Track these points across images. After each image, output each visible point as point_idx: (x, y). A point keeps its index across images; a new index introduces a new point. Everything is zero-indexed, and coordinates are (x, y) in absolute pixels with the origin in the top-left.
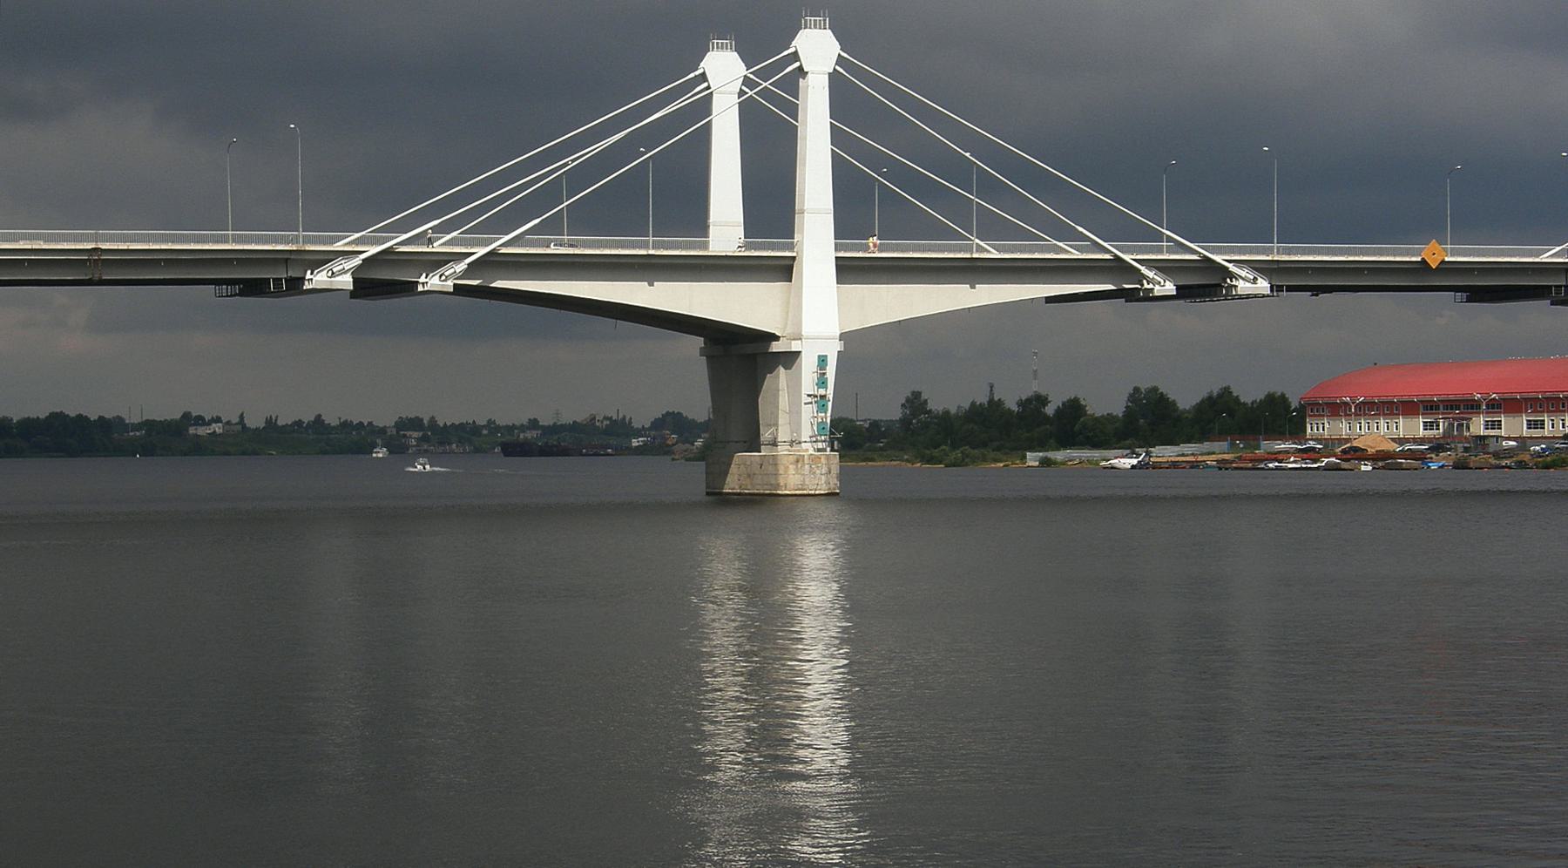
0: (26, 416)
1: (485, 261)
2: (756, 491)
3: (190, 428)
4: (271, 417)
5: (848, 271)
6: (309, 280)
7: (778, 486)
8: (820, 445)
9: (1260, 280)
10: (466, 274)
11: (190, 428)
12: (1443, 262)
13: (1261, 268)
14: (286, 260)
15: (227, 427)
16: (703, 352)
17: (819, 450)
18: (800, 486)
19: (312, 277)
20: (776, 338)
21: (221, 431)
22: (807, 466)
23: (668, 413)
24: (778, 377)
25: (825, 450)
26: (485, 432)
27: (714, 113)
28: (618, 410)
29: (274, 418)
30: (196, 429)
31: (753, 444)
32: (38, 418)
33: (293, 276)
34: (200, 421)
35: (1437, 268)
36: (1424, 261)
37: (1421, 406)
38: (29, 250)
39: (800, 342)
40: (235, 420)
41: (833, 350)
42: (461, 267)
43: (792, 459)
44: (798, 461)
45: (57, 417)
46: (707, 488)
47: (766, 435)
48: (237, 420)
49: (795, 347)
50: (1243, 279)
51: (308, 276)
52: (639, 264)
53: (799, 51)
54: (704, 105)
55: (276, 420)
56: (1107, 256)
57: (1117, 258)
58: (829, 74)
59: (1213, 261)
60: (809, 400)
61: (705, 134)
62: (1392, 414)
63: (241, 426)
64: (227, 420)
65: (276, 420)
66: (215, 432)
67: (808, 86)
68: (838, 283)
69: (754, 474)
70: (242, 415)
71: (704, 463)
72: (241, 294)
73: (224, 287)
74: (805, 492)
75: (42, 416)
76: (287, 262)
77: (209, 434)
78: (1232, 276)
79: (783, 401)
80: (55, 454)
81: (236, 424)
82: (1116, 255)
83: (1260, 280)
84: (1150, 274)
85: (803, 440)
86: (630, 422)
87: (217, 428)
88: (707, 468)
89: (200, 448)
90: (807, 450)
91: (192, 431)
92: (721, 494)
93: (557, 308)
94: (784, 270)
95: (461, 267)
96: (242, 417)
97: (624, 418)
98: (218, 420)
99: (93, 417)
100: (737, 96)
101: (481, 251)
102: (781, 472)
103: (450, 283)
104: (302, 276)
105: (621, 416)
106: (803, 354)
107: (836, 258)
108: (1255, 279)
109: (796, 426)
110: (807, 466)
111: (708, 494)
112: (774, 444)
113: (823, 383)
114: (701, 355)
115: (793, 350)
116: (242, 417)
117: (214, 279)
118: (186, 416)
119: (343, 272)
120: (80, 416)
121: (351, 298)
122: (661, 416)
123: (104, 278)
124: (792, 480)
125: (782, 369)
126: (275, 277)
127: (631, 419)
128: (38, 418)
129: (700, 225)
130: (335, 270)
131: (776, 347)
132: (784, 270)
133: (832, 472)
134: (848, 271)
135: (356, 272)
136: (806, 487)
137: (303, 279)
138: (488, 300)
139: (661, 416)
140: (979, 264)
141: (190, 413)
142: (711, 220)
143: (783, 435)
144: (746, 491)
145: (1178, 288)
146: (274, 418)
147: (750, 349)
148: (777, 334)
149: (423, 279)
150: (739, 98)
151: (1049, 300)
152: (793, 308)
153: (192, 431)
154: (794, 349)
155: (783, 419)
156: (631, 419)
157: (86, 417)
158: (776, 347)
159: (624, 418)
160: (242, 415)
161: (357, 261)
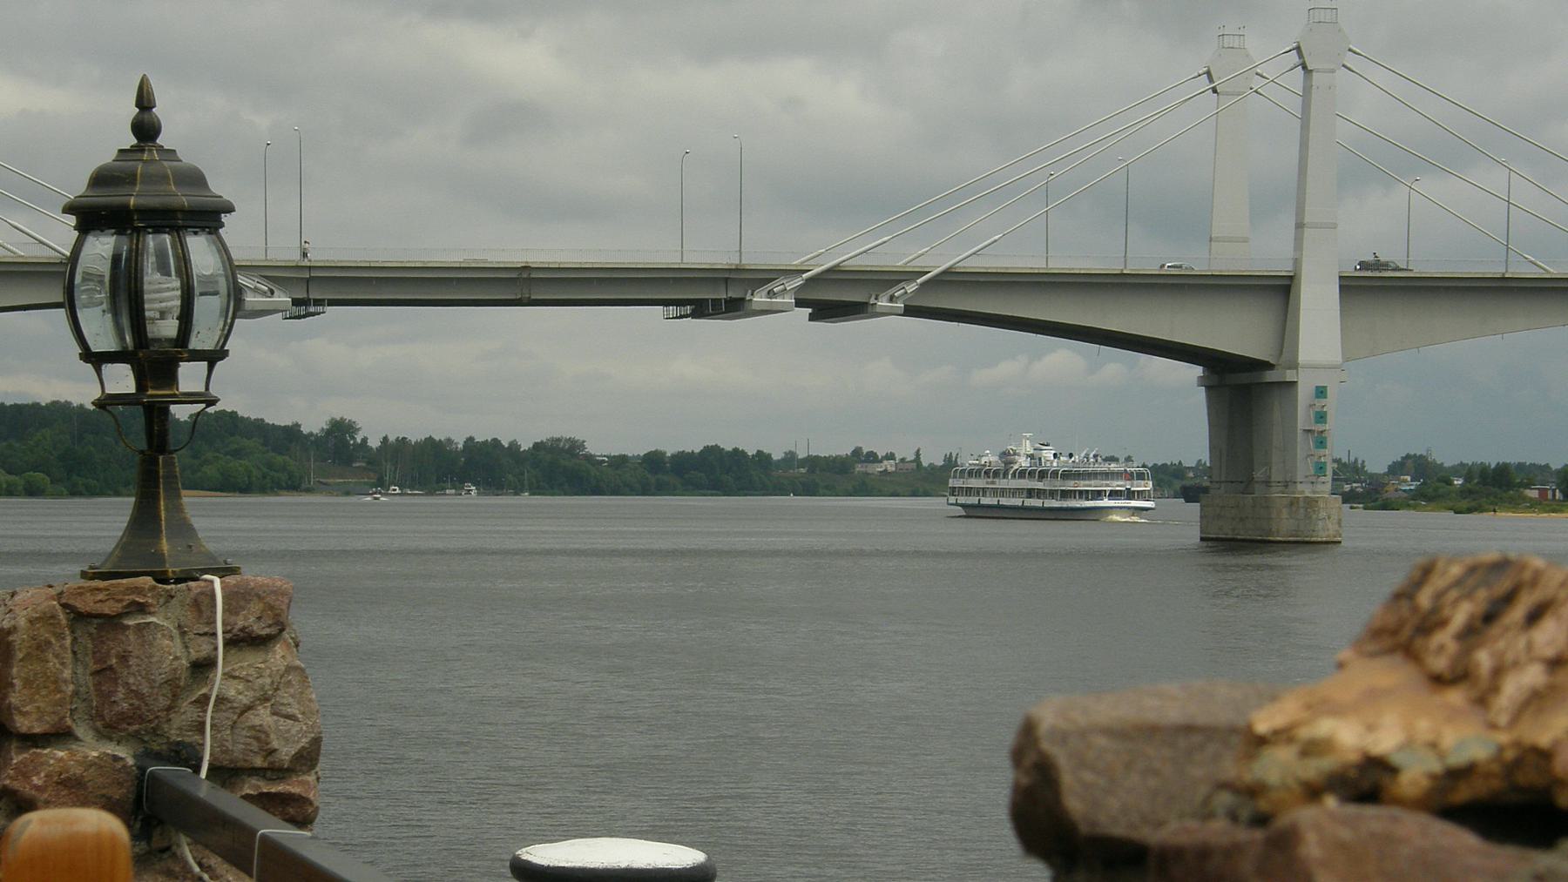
0: (681, 450)
1: (818, 279)
2: (1248, 537)
3: (856, 465)
4: (951, 453)
6: (872, 304)
9: (276, 292)
11: (856, 465)
14: (726, 280)
15: (901, 465)
16: (1202, 381)
18: (1294, 533)
19: (751, 297)
21: (894, 469)
22: (1302, 511)
23: (1408, 457)
26: (1191, 475)
28: (1349, 451)
29: (954, 456)
30: (866, 467)
32: (693, 452)
33: (734, 296)
34: (872, 458)
38: (456, 268)
39: (1295, 371)
40: (911, 457)
42: (911, 288)
44: (1292, 504)
45: (712, 452)
46: (1201, 532)
47: (1259, 475)
48: (912, 457)
52: (675, 279)
53: (1301, 45)
55: (956, 458)
63: (915, 464)
64: (901, 457)
65: (956, 458)
66: (886, 470)
67: (1312, 86)
69: (1247, 518)
70: (918, 450)
71: (1199, 504)
72: (694, 315)
73: (671, 308)
74: (1299, 539)
75: (697, 451)
76: (308, 281)
77: (881, 472)
80: (709, 492)
81: (911, 462)
85: (1299, 480)
86: (1363, 467)
87: (889, 466)
88: (1201, 510)
89: (864, 488)
90: (1303, 492)
91: (859, 468)
93: (1033, 333)
95: (911, 288)
96: (918, 454)
97: (1356, 460)
98: (891, 457)
99: (751, 452)
102: (1273, 516)
104: (743, 296)
105: (1352, 459)
106: (1299, 382)
107: (1340, 277)
108: (272, 292)
110: (1302, 511)
111: (1202, 539)
112: (1267, 483)
113: (1322, 417)
114: (1198, 386)
115: (1288, 380)
116: (918, 454)
117: (675, 300)
118: (857, 452)
120: (736, 450)
121: (810, 320)
122: (1399, 460)
123: (533, 297)
126: (714, 297)
127: (1363, 462)
128: (693, 452)
131: (1271, 376)
133: (1332, 517)
136: (1300, 533)
138: (956, 323)
139: (1399, 460)
140: (1514, 285)
141: (861, 448)
143: (1276, 476)
144: (1239, 537)
146: (954, 456)
147: (1244, 378)
148: (1272, 362)
153: (859, 468)
156: (1363, 462)
157: (743, 451)
159: (1356, 460)
160: (918, 450)
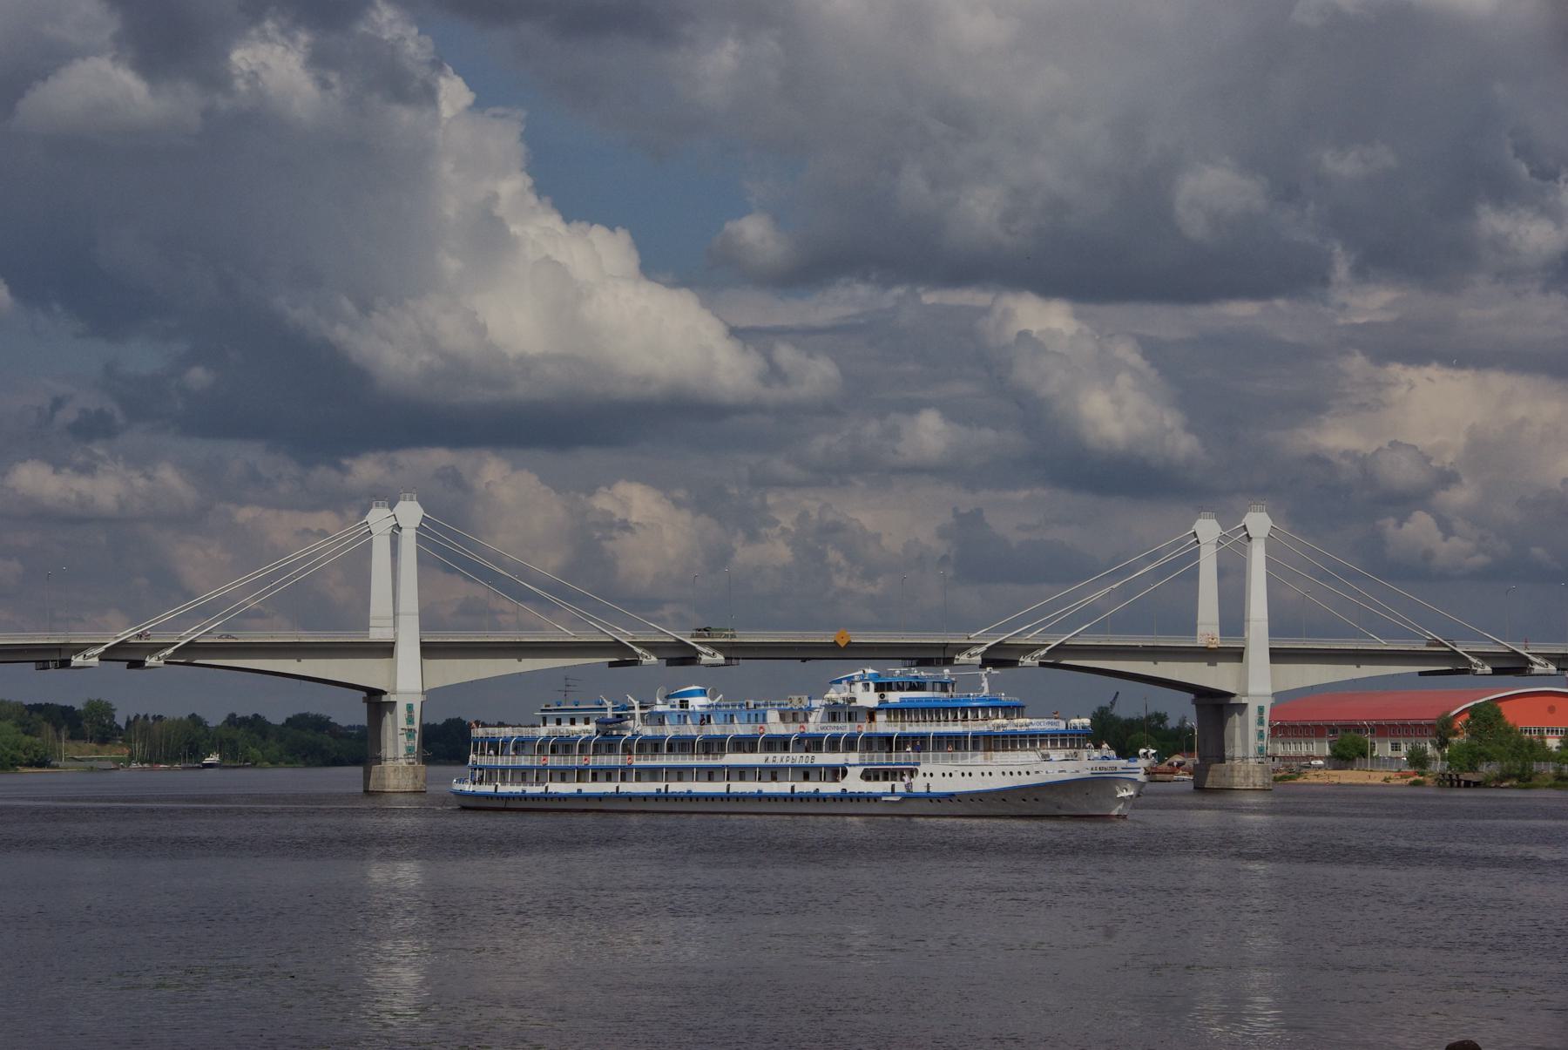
5: (1277, 655)
7: (384, 786)
8: (411, 760)
10: (1046, 656)
12: (849, 643)
13: (1550, 658)
16: (1194, 702)
17: (409, 763)
20: (385, 693)
24: (1234, 721)
25: (413, 763)
27: (1201, 559)
31: (1222, 759)
35: (845, 647)
36: (835, 643)
37: (1327, 730)
41: (1267, 704)
42: (1043, 652)
43: (393, 769)
44: (395, 770)
49: (1244, 700)
50: (705, 654)
51: (957, 657)
54: (1195, 554)
56: (1446, 649)
57: (617, 641)
58: (1265, 539)
59: (1519, 653)
60: (404, 732)
61: (1196, 570)
62: (1309, 736)
68: (1271, 663)
78: (698, 652)
79: (1238, 731)
82: (1452, 649)
83: (1550, 665)
84: (1475, 661)
90: (401, 764)
92: (1204, 788)
94: (1237, 655)
95: (1043, 652)
100: (1215, 547)
101: (1055, 644)
103: (1037, 662)
107: (1270, 649)
108: (714, 654)
109: (396, 749)
119: (976, 654)
124: (1238, 781)
125: (1236, 715)
129: (1192, 629)
130: (972, 653)
131: (1233, 701)
132: (1237, 655)
134: (1277, 655)
135: (983, 654)
137: (953, 658)
142: (1199, 621)
143: (1238, 752)
145: (1493, 669)
149: (1021, 659)
150: (1217, 548)
151: (1421, 674)
152: (1243, 679)
154: (392, 700)
155: (1238, 741)
158: (1233, 701)
161: (984, 649)
